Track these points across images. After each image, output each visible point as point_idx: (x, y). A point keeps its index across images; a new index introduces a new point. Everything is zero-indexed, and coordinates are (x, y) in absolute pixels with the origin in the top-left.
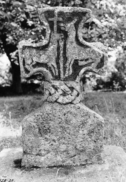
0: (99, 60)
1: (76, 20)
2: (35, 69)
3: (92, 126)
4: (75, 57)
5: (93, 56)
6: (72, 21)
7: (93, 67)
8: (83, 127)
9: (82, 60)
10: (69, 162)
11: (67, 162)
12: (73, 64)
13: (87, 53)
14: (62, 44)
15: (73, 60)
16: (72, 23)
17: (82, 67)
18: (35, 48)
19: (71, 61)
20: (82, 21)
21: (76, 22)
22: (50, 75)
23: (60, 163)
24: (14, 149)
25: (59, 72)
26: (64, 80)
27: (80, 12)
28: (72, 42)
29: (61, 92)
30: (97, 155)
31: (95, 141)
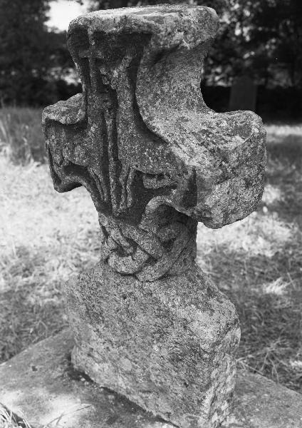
0: (184, 185)
1: (129, 58)
2: (68, 177)
3: (178, 346)
4: (134, 165)
5: (171, 170)
6: (120, 62)
7: (174, 200)
8: (161, 339)
9: (151, 176)
10: (134, 397)
11: (135, 397)
12: (134, 179)
13: (157, 159)
14: (109, 122)
15: (132, 171)
16: (121, 68)
17: (152, 193)
18: (65, 126)
19: (128, 176)
20: (142, 62)
21: (131, 64)
22: (112, 190)
23: (123, 393)
24: (128, 396)
25: (109, 196)
26: (117, 218)
27: (135, 34)
28: (126, 124)
29: (113, 246)
30: (189, 415)
31: (185, 384)
